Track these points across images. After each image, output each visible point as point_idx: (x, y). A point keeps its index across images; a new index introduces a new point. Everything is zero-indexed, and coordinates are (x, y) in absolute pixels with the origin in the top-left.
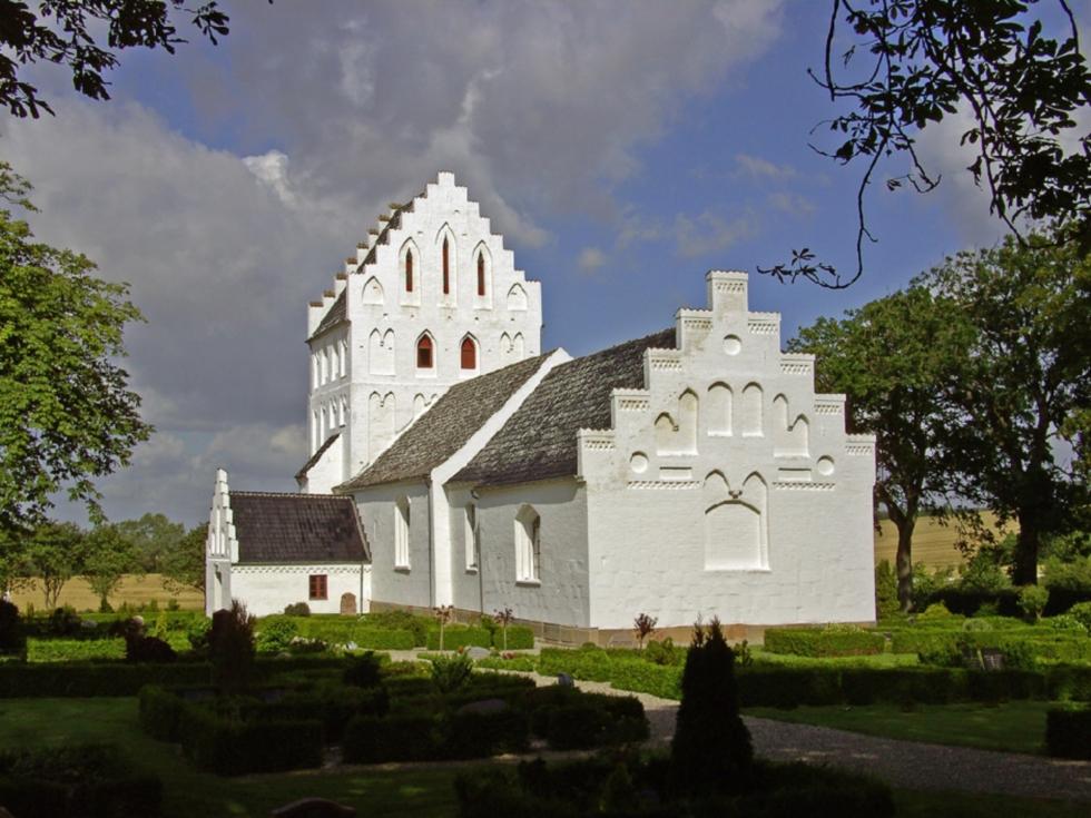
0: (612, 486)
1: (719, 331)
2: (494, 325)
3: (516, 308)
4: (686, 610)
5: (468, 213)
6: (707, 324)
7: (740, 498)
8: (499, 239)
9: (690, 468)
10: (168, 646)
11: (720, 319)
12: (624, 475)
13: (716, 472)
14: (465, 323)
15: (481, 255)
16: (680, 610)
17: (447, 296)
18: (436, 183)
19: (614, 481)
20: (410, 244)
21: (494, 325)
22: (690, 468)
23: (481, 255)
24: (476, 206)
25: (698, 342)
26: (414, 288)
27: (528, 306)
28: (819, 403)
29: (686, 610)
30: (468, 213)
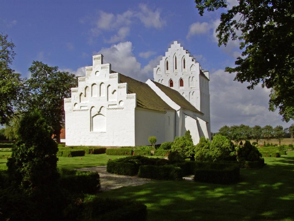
0: (70, 111)
1: (94, 71)
2: (187, 75)
3: (193, 70)
4: (86, 142)
5: (181, 49)
6: (91, 70)
7: (100, 113)
8: (188, 54)
9: (87, 106)
10: (259, 152)
11: (94, 67)
12: (72, 109)
13: (81, 107)
14: (180, 75)
15: (184, 59)
16: (84, 141)
17: (177, 70)
18: (173, 44)
19: (70, 110)
20: (167, 59)
21: (187, 75)
22: (87, 106)
23: (184, 59)
24: (182, 47)
25: (89, 74)
26: (169, 69)
27: (196, 70)
28: (119, 86)
29: (86, 142)
30: (181, 49)
